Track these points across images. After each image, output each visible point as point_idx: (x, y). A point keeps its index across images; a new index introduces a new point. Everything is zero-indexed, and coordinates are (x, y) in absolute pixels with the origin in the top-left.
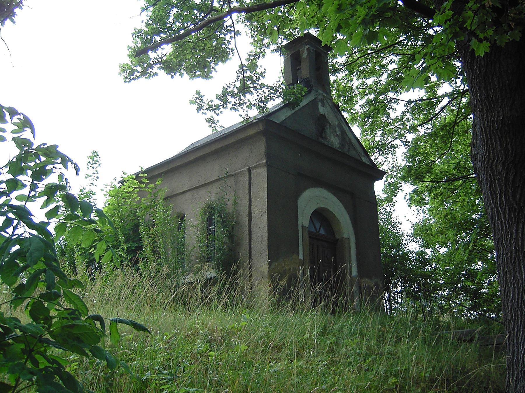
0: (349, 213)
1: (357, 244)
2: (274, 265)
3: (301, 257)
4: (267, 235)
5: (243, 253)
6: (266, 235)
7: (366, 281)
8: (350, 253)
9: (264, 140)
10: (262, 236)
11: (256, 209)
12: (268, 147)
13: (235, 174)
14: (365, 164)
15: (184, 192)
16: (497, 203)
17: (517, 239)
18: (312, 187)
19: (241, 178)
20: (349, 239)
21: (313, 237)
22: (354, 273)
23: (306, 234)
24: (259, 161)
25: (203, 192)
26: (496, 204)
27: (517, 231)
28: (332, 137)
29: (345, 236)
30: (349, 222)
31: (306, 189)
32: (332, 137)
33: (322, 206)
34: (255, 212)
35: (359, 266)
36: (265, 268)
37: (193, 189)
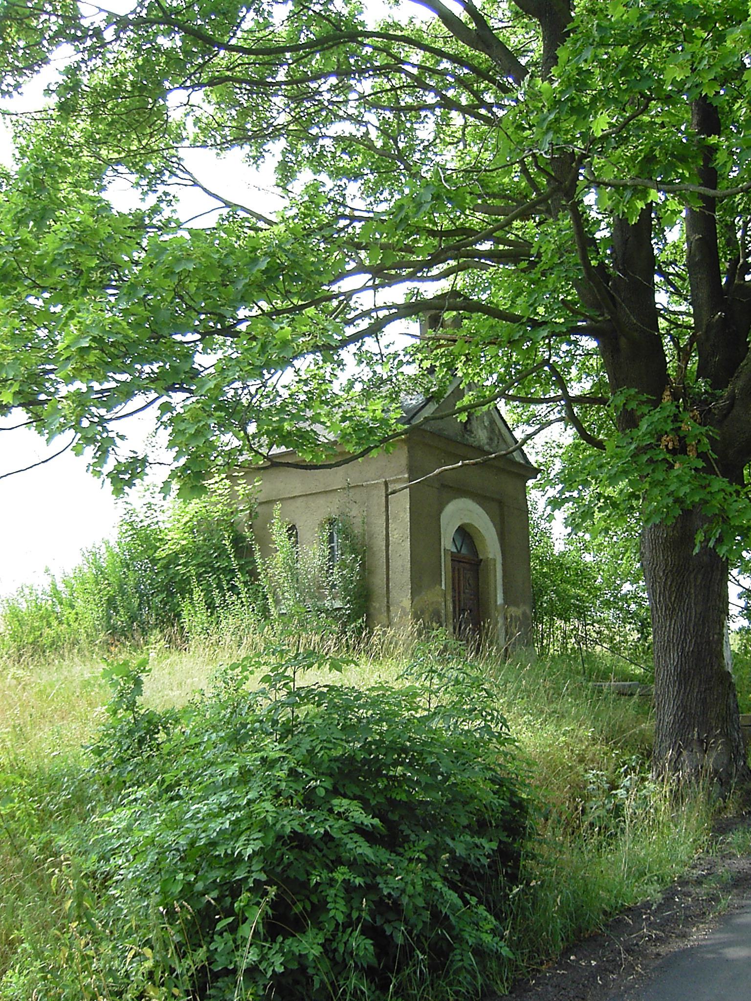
0: (495, 526)
1: (504, 565)
2: (416, 599)
3: (443, 587)
4: (409, 566)
5: (379, 580)
6: (408, 566)
7: (514, 611)
8: (495, 576)
9: (406, 448)
10: (403, 566)
11: (395, 533)
12: (411, 457)
13: (367, 486)
14: (521, 464)
15: (388, 579)
16: (655, 601)
17: (669, 632)
18: (455, 498)
19: (375, 492)
20: (495, 560)
21: (456, 559)
22: (500, 601)
23: (449, 558)
24: (398, 474)
25: (321, 501)
26: (655, 601)
27: (670, 625)
28: (479, 430)
29: (491, 556)
30: (496, 537)
31: (448, 503)
32: (479, 430)
33: (467, 521)
34: (394, 537)
35: (505, 593)
36: (407, 603)
37: (306, 495)
